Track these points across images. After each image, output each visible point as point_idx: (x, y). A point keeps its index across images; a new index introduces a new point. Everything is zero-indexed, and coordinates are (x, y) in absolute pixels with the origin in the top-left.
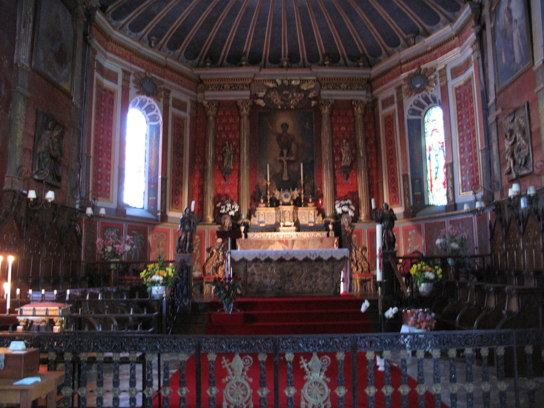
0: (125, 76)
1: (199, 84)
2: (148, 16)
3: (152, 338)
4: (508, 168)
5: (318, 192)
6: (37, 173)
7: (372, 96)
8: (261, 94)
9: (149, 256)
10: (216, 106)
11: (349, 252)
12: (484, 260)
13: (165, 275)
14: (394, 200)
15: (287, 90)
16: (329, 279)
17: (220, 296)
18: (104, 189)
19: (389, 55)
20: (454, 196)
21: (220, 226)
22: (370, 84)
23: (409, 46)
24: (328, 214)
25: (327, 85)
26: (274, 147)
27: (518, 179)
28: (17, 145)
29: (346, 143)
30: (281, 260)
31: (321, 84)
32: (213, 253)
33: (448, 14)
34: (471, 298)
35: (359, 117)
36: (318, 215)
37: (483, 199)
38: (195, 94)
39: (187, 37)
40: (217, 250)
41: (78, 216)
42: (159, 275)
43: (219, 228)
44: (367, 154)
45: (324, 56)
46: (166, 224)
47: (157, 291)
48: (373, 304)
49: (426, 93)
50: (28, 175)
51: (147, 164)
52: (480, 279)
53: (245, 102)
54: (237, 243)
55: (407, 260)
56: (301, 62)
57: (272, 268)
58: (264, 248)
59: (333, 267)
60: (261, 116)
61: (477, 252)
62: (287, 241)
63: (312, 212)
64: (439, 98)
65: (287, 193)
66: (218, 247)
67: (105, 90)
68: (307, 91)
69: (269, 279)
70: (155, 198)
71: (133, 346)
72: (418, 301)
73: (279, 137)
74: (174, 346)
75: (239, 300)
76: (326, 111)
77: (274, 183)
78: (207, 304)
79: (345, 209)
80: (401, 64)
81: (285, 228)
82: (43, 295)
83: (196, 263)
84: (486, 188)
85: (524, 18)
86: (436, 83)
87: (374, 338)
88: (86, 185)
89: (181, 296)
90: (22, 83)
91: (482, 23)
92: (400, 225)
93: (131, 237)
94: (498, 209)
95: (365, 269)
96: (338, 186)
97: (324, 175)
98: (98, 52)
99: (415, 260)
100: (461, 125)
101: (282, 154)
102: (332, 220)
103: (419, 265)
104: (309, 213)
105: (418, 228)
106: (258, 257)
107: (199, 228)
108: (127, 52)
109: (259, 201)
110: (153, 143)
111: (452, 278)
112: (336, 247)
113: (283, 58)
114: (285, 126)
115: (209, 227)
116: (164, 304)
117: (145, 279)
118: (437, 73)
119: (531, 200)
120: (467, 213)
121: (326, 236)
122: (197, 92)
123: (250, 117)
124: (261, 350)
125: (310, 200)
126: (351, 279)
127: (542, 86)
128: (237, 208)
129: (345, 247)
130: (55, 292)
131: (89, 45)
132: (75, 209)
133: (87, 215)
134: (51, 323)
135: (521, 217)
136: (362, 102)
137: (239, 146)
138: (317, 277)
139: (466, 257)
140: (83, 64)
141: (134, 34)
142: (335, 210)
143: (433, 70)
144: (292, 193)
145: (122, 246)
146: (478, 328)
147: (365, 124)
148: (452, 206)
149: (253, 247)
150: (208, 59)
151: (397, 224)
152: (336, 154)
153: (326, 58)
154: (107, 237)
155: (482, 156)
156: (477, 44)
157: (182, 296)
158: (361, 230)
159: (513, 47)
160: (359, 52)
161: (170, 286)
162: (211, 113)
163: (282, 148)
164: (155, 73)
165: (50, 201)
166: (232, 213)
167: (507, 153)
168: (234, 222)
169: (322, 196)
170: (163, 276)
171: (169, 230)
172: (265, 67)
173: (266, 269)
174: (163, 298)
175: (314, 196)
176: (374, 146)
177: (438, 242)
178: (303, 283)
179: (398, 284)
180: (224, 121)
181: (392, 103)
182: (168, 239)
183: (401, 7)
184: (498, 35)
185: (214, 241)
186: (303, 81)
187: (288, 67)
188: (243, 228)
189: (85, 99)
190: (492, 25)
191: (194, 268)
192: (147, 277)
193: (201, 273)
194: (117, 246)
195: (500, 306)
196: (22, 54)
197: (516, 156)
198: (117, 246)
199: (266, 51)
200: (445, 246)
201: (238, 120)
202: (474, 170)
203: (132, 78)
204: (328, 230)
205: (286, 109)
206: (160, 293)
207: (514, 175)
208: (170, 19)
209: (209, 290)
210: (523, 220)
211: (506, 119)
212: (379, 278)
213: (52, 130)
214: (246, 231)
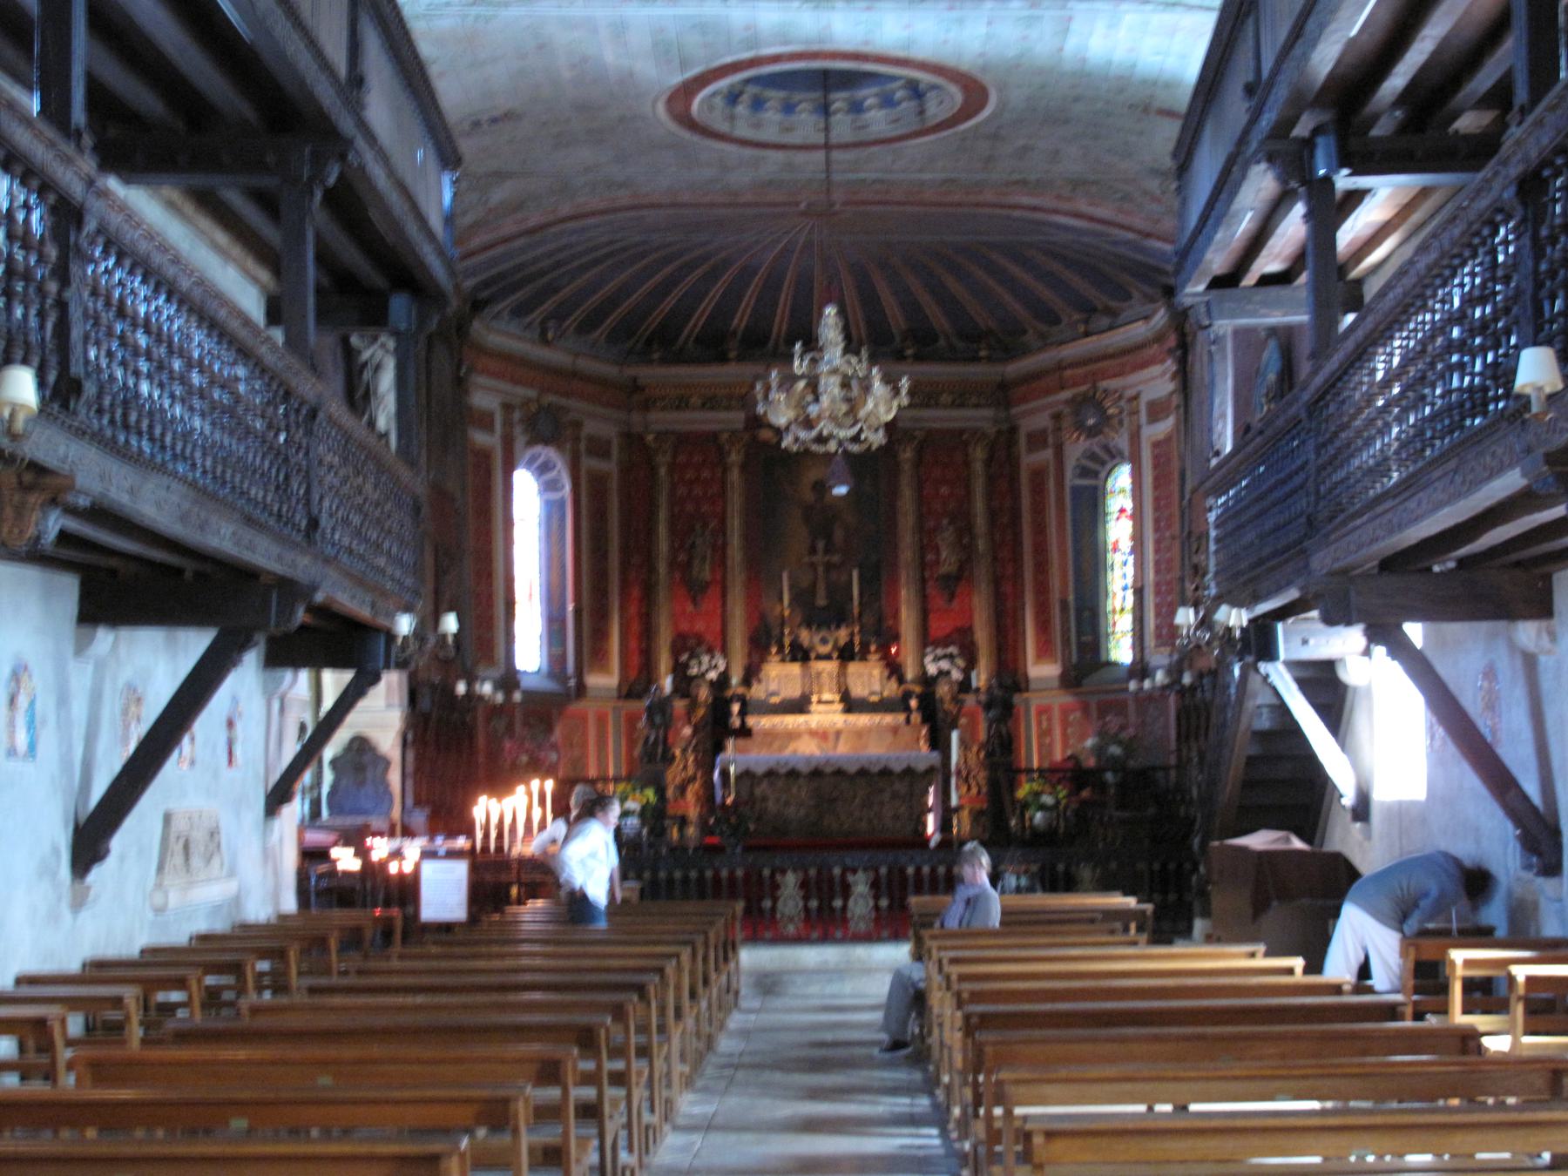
1: (634, 395)
22: (1004, 394)
24: (910, 674)
30: (817, 773)
35: (978, 467)
36: (889, 678)
79: (944, 665)
81: (822, 707)
102: (918, 689)
104: (871, 675)
105: (1085, 709)
123: (744, 468)
137: (722, 530)
138: (882, 803)
142: (923, 666)
147: (991, 480)
148: (1140, 669)
152: (926, 546)
166: (713, 675)
169: (896, 638)
181: (1044, 444)
188: (736, 708)
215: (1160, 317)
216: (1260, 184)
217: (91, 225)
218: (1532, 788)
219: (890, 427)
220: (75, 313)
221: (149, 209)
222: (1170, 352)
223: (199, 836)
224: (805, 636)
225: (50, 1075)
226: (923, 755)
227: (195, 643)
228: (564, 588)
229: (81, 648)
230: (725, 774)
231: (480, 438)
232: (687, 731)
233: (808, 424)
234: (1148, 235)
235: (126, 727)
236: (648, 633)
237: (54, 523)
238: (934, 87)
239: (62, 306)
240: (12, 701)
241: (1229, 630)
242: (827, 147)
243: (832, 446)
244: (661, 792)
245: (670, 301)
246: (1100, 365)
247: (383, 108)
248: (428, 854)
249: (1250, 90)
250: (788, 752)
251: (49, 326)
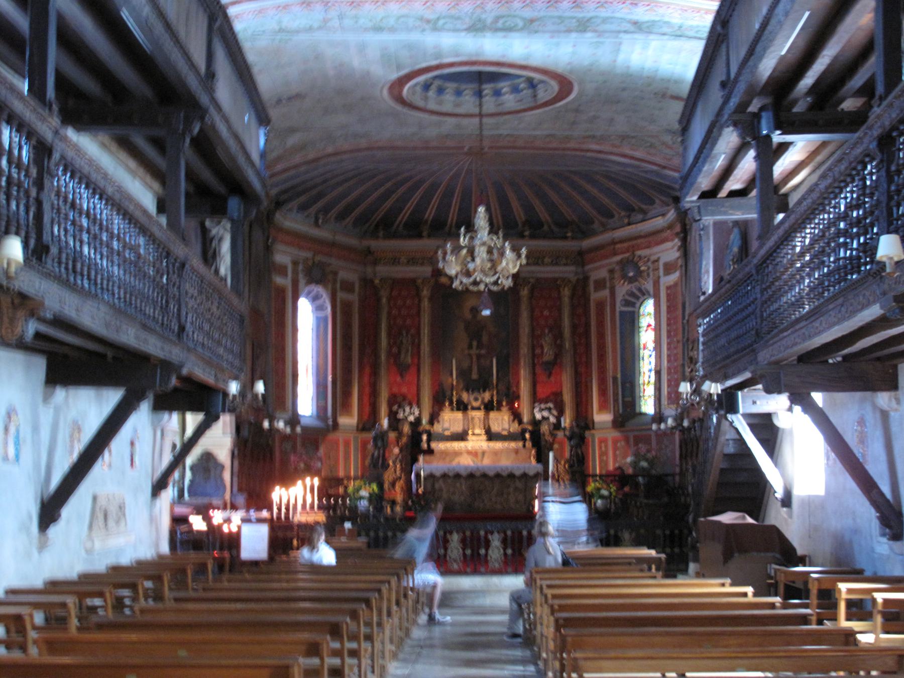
1: (368, 256)
22: (581, 258)
24: (525, 419)
26: (461, 336)
30: (471, 476)
36: (513, 421)
44: (575, 346)
47: (363, 504)
64: (652, 292)
65: (476, 394)
79: (546, 414)
81: (474, 438)
86: (648, 275)
97: (522, 372)
101: (470, 347)
104: (503, 419)
105: (627, 439)
112: (533, 461)
123: (431, 299)
125: (504, 403)
128: (417, 413)
138: (509, 494)
147: (573, 307)
148: (659, 417)
156: (682, 249)
162: (384, 295)
166: (411, 418)
169: (517, 398)
181: (604, 287)
188: (425, 437)
201: (416, 302)
203: (301, 267)
215: (671, 215)
216: (729, 139)
217: (56, 156)
218: (886, 489)
219: (515, 277)
220: (46, 207)
221: (90, 147)
222: (677, 234)
223: (113, 510)
224: (465, 396)
225: (23, 648)
226: (533, 466)
227: (113, 397)
228: (326, 370)
229: (46, 398)
230: (418, 476)
231: (279, 280)
232: (396, 450)
233: (468, 274)
234: (664, 167)
235: (72, 441)
236: (374, 394)
237: (32, 328)
238: (542, 82)
239: (39, 203)
240: (6, 429)
241: (711, 395)
242: (481, 115)
243: (482, 287)
244: (381, 486)
245: (388, 204)
247: (225, 90)
248: (246, 520)
249: (723, 85)
251: (31, 214)
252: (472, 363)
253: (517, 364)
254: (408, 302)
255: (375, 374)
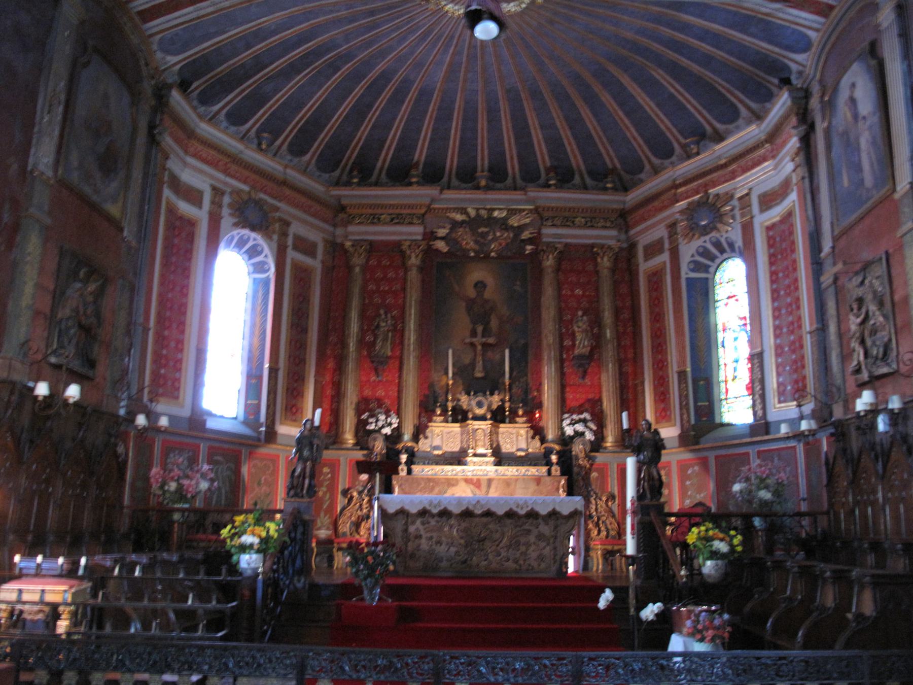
0: (215, 197)
1: (339, 213)
2: (257, 100)
3: (220, 647)
4: (855, 363)
5: (534, 398)
6: (54, 352)
7: (628, 239)
8: (442, 232)
9: (243, 502)
10: (365, 250)
11: (583, 502)
12: (815, 522)
13: (264, 534)
14: (664, 414)
15: (486, 227)
16: (548, 548)
17: (356, 574)
18: (170, 383)
19: (656, 171)
20: (764, 408)
21: (365, 452)
22: (624, 219)
23: (689, 156)
24: (550, 436)
25: (554, 218)
27: (873, 382)
28: (24, 304)
29: (582, 316)
30: (467, 514)
31: (542, 218)
32: (352, 497)
33: (753, 105)
34: (792, 589)
35: (605, 273)
36: (533, 438)
37: (814, 415)
38: (331, 229)
39: (322, 136)
40: (360, 493)
41: (123, 428)
42: (253, 534)
43: (364, 455)
44: (619, 337)
45: (548, 170)
46: (274, 446)
47: (248, 561)
48: (620, 593)
49: (718, 235)
50: (39, 357)
51: (246, 343)
52: (810, 554)
53: (414, 244)
54: (394, 482)
55: (683, 519)
56: (509, 180)
57: (451, 527)
58: (440, 493)
59: (556, 527)
60: (441, 268)
61: (804, 507)
62: (478, 480)
63: (523, 432)
64: (739, 243)
65: (480, 398)
66: (361, 489)
67: (181, 218)
68: (519, 227)
69: (446, 546)
70: (256, 402)
71: (186, 662)
72: (701, 590)
73: (471, 304)
74: (259, 665)
75: (390, 581)
76: (549, 262)
77: (461, 382)
78: (337, 585)
79: (580, 427)
80: (676, 186)
82: (39, 565)
83: (322, 514)
84: (819, 396)
85: (878, 114)
86: (733, 217)
87: (613, 660)
88: (139, 377)
89: (291, 572)
90: (40, 201)
91: (809, 122)
92: (673, 456)
93: (211, 467)
94: (840, 432)
95: (613, 533)
96: (568, 389)
97: (545, 369)
98: (172, 156)
99: (697, 519)
100: (775, 286)
101: (474, 334)
103: (703, 528)
104: (518, 435)
105: (704, 462)
106: (428, 508)
107: (328, 454)
108: (220, 157)
109: (434, 412)
110: (257, 309)
111: (760, 552)
112: (562, 494)
113: (478, 174)
114: (480, 286)
115: (348, 454)
116: (260, 586)
117: (228, 541)
118: (735, 202)
119: (895, 418)
120: (787, 438)
121: (546, 474)
122: (335, 226)
123: (421, 269)
124: (412, 677)
125: (520, 412)
126: (587, 549)
127: (908, 225)
128: (395, 421)
129: (579, 495)
130: (61, 560)
131: (158, 144)
132: (118, 416)
133: (136, 427)
134: (54, 613)
135: (878, 448)
136: (610, 248)
137: (402, 318)
138: (528, 545)
139: (784, 515)
140: (146, 175)
141: (233, 129)
142: (561, 429)
143: (730, 197)
144: (490, 399)
145: (193, 482)
146: (805, 647)
147: (616, 285)
148: (762, 426)
149: (420, 491)
150: (355, 173)
151: (665, 456)
152: (565, 334)
153: (552, 174)
154: (170, 466)
155: (812, 343)
156: (802, 154)
157: (293, 571)
158: (606, 465)
159: (860, 160)
160: (605, 163)
161: (272, 554)
162: (358, 261)
163: (474, 323)
164: (265, 193)
165: (71, 401)
166: (387, 431)
167: (852, 338)
168: (390, 446)
169: (540, 406)
170: (260, 536)
171: (278, 456)
172: (449, 188)
173: (440, 529)
174: (258, 575)
175: (526, 405)
176: (631, 323)
177: (737, 487)
178: (503, 554)
179: (666, 560)
180: (379, 274)
181: (661, 251)
182: (275, 472)
183: (676, 94)
184: (836, 141)
185: (354, 479)
186: (512, 212)
187: (488, 188)
188: (404, 458)
189: (145, 231)
190: (825, 125)
191: (319, 524)
192: (232, 537)
193: (330, 532)
194: (186, 482)
195: (844, 604)
196: (43, 157)
197: (869, 342)
198: (186, 482)
199: (452, 161)
200: (748, 494)
202: (798, 365)
203: (226, 200)
204: (549, 463)
205: (483, 257)
206: (253, 565)
207: (865, 376)
208: (294, 104)
209: (342, 559)
210: (883, 453)
211: (850, 279)
212: (630, 549)
213: (86, 281)
214: (410, 463)
224: (464, 401)
236: (338, 396)
245: (363, 132)
246: (709, 177)
250: (447, 495)
252: (475, 355)
253: (539, 358)
254: (391, 274)
255: (340, 369)
